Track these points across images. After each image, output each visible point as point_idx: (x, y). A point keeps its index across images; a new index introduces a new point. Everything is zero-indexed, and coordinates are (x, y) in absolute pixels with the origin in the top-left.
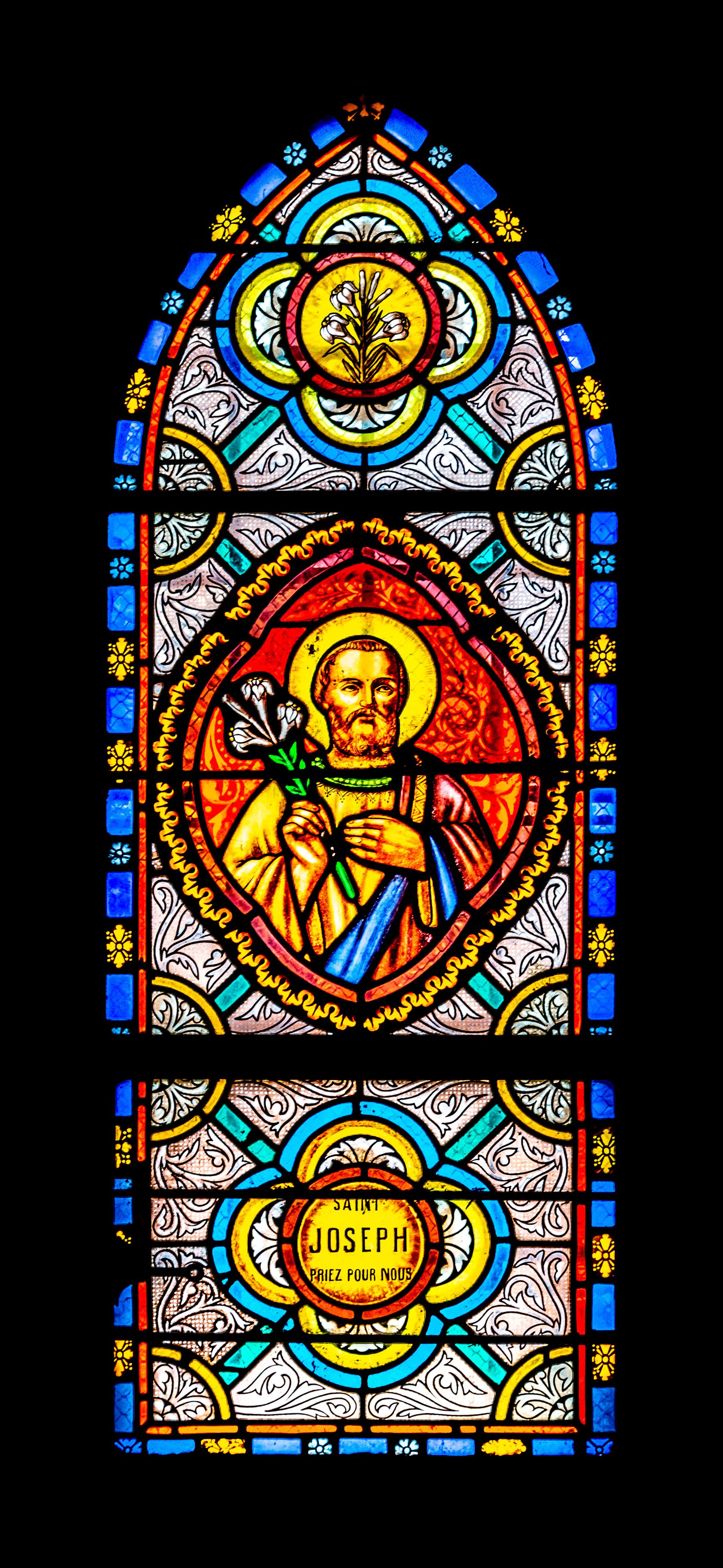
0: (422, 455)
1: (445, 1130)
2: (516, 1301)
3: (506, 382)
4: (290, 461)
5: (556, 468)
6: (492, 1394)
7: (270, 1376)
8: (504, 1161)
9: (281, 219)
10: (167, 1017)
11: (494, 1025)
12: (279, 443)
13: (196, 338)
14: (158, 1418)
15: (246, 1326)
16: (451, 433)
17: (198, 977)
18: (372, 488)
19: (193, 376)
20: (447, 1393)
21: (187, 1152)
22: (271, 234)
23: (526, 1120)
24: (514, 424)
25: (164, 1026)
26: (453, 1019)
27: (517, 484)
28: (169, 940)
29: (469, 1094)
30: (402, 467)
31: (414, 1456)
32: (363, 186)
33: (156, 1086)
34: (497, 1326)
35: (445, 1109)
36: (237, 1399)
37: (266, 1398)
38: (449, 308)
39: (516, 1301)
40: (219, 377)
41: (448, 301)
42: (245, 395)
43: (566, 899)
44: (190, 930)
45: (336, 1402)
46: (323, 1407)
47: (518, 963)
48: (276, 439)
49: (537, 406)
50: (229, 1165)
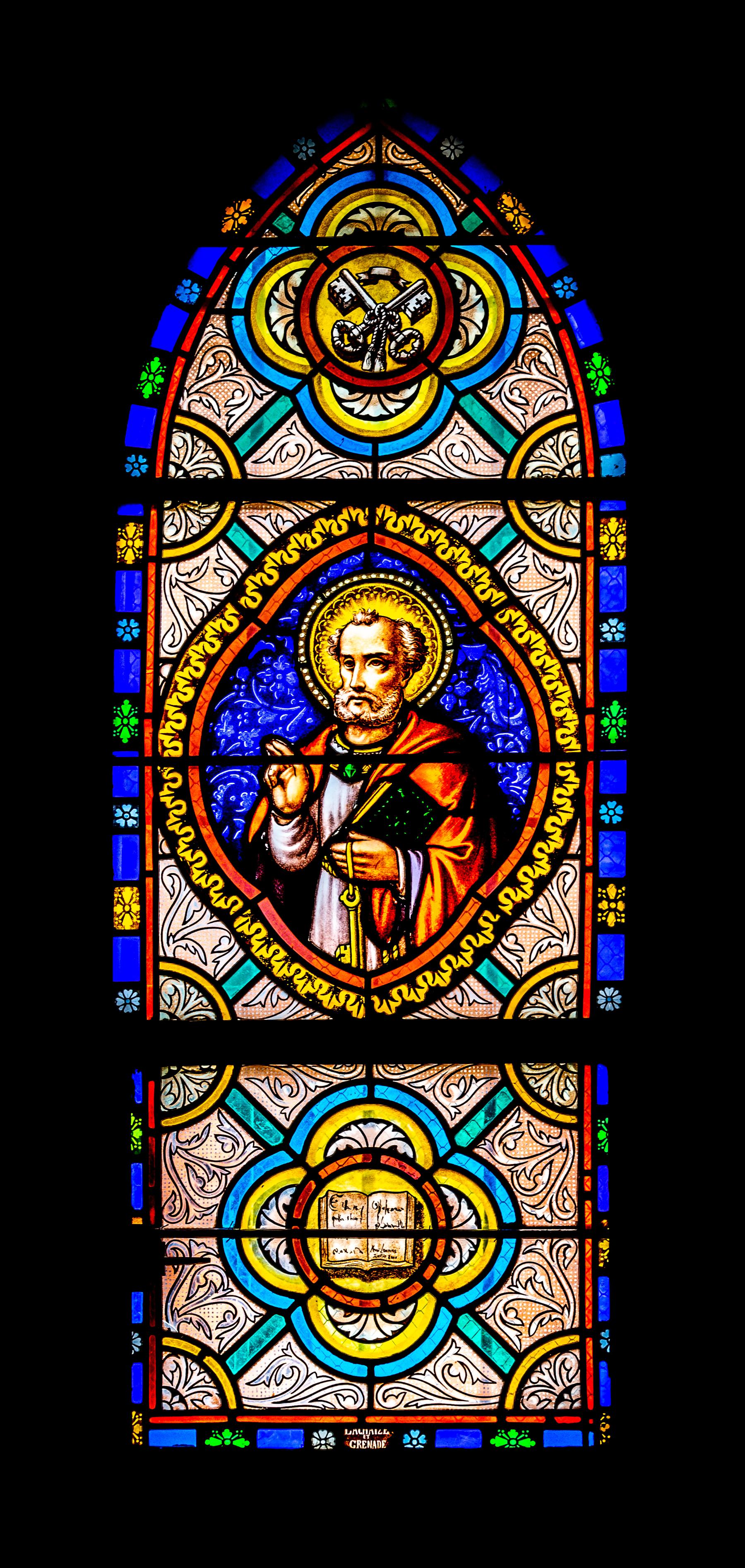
0: (311, 1096)
1: (456, 1113)
2: (525, 1288)
3: (520, 372)
4: (445, 1089)
5: (567, 456)
6: (500, 1383)
7: (280, 1367)
8: (511, 1145)
9: (294, 207)
10: (175, 1002)
11: (503, 1011)
12: (291, 434)
13: (210, 329)
14: (166, 1407)
15: (255, 1317)
16: (463, 423)
17: (206, 964)
18: (384, 476)
19: (208, 366)
20: (455, 1382)
21: (546, 402)
22: (284, 223)
23: (536, 1106)
24: (527, 413)
25: (172, 1010)
26: (278, 515)
27: (529, 471)
28: (177, 924)
29: (478, 1076)
30: (331, 1083)
31: (420, 1449)
32: (371, 1371)
33: (165, 1072)
34: (506, 1312)
35: (456, 1092)
36: (245, 1391)
37: (274, 1389)
38: (462, 298)
39: (525, 1288)
40: (234, 366)
41: (460, 291)
42: (260, 384)
43: (576, 885)
44: (197, 916)
45: (345, 1393)
46: (331, 1398)
47: (211, 570)
48: (288, 429)
49: (193, 1145)
50: (506, 389)
